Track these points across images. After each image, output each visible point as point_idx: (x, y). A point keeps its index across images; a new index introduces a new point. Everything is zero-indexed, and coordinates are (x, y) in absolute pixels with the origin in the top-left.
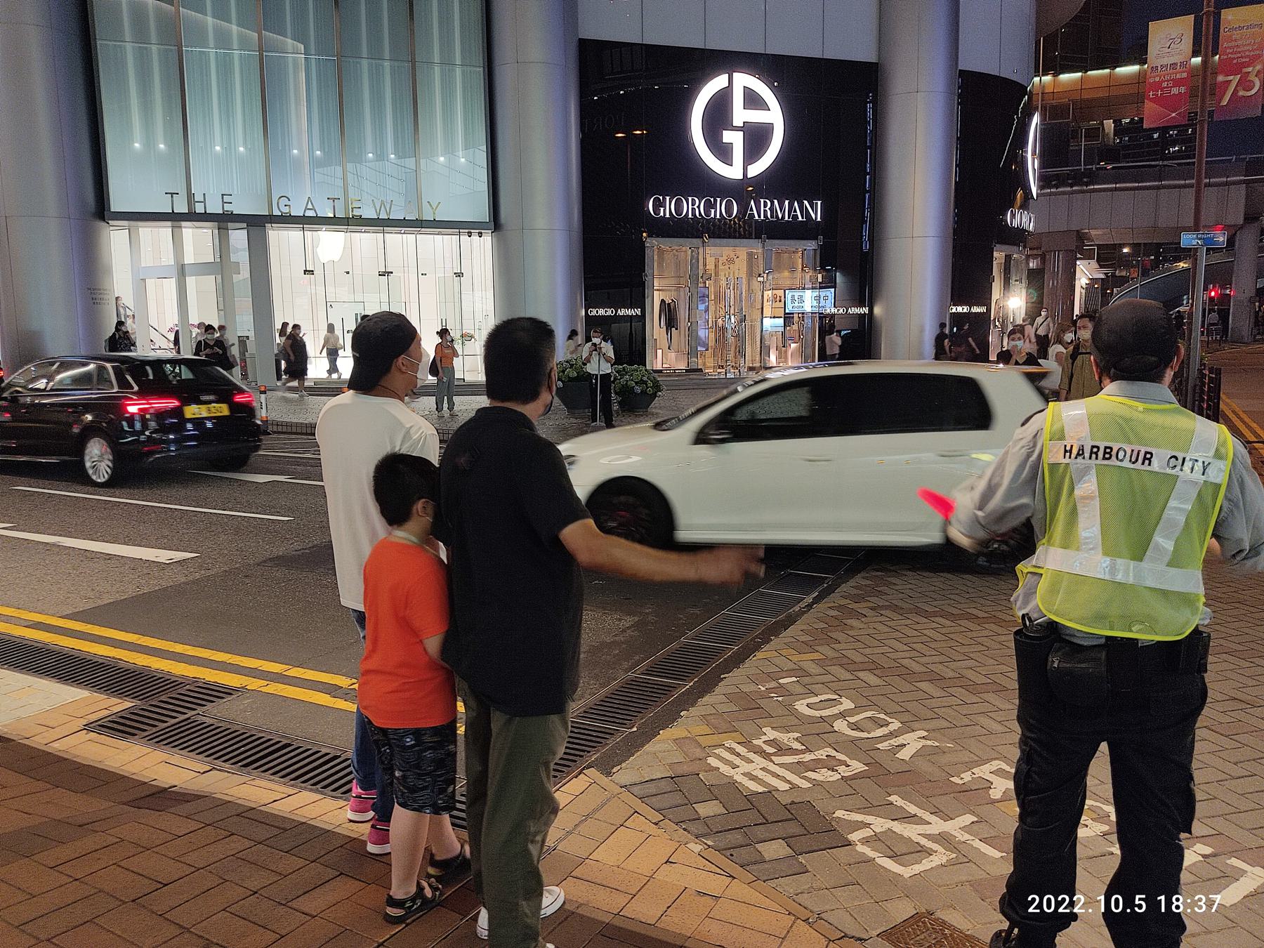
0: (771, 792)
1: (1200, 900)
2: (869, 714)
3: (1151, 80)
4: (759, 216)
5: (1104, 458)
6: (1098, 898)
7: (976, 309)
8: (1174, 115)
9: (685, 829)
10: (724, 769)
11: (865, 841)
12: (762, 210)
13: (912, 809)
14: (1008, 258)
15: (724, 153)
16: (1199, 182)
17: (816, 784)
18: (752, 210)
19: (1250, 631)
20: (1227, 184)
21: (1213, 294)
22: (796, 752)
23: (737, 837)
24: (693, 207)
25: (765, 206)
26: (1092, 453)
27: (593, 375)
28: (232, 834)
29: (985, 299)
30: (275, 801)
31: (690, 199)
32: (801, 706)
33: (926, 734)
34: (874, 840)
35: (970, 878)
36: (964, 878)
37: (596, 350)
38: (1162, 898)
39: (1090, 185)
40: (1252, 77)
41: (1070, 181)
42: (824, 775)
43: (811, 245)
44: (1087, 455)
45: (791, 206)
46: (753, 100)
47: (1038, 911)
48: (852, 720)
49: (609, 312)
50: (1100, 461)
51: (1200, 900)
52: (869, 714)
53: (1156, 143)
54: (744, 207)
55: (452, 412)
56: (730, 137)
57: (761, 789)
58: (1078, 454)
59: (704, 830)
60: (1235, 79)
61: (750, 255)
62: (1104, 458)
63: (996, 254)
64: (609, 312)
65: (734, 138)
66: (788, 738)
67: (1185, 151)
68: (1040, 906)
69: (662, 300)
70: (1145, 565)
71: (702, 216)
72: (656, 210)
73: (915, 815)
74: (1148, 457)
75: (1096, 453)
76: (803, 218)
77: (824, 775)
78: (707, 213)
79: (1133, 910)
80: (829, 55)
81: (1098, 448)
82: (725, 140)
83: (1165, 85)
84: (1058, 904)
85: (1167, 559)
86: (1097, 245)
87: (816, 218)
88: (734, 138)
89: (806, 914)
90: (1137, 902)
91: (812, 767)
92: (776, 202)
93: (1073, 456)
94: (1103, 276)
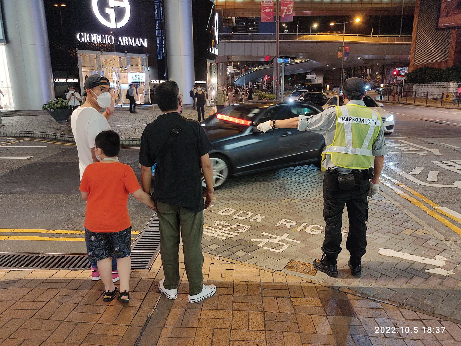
0: (229, 238)
2: (242, 212)
3: (262, 6)
5: (353, 121)
7: (203, 82)
8: (269, 18)
9: (210, 254)
10: (210, 235)
11: (264, 246)
12: (124, 41)
13: (271, 235)
14: (211, 64)
15: (107, 17)
16: (277, 40)
17: (240, 234)
18: (120, 41)
19: (299, 180)
20: (271, 42)
21: (267, 78)
22: (228, 226)
23: (228, 253)
24: (96, 38)
26: (350, 119)
27: (72, 106)
28: (48, 289)
29: (205, 80)
30: (53, 275)
32: (220, 213)
33: (260, 215)
34: (265, 245)
35: (297, 249)
36: (295, 250)
37: (73, 96)
39: (231, 40)
40: (290, 8)
41: (224, 38)
42: (240, 231)
43: (144, 56)
44: (348, 120)
47: (379, 332)
48: (238, 214)
49: (64, 80)
50: (352, 122)
51: (438, 328)
52: (242, 212)
53: (244, 27)
54: (117, 40)
55: (2, 124)
56: (108, 11)
57: (226, 238)
58: (346, 120)
59: (216, 253)
60: (286, 8)
61: (120, 58)
62: (353, 121)
63: (207, 63)
64: (64, 80)
65: (111, 12)
66: (223, 223)
67: (253, 30)
69: (86, 76)
70: (361, 149)
73: (272, 237)
74: (363, 121)
75: (351, 120)
77: (240, 231)
81: (351, 118)
83: (266, 8)
84: (386, 330)
85: (367, 147)
86: (233, 61)
88: (111, 12)
89: (261, 268)
91: (236, 229)
93: (345, 121)
94: (234, 72)
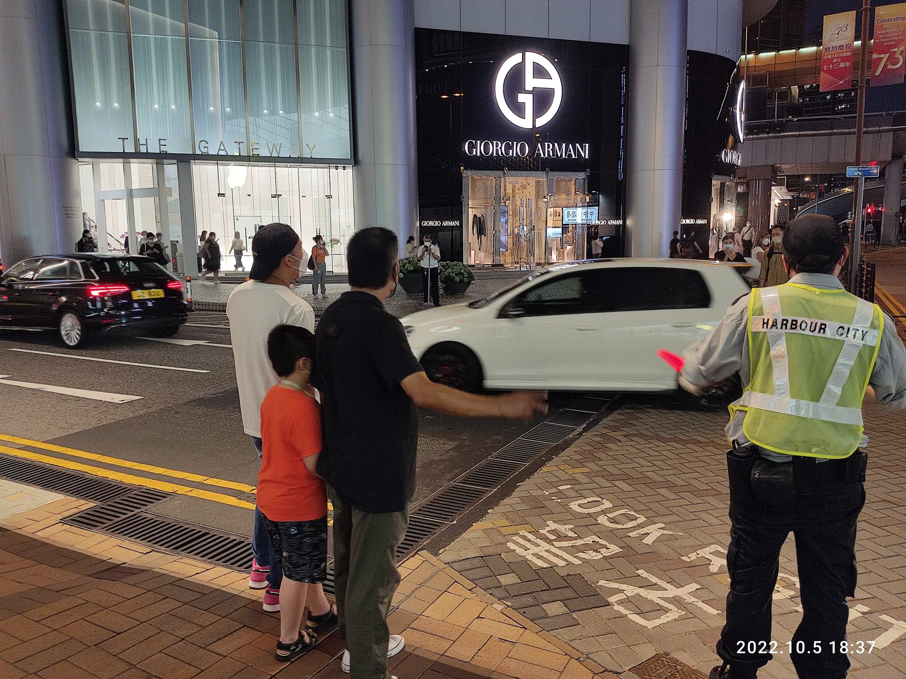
0: (552, 567)
1: (860, 644)
2: (623, 511)
3: (825, 58)
4: (544, 155)
5: (791, 328)
6: (787, 643)
7: (699, 222)
8: (841, 82)
9: (491, 594)
10: (519, 551)
11: (620, 602)
12: (546, 150)
13: (654, 579)
14: (723, 185)
15: (519, 110)
16: (859, 131)
17: (585, 561)
18: (539, 150)
19: (896, 452)
20: (879, 132)
21: (869, 210)
22: (571, 539)
23: (528, 600)
24: (497, 148)
25: (549, 147)
26: (782, 324)
27: (425, 268)
28: (166, 598)
29: (706, 214)
30: (197, 574)
31: (495, 142)
32: (574, 506)
33: (664, 525)
34: (627, 602)
35: (696, 629)
36: (691, 629)
37: (427, 251)
38: (833, 643)
39: (781, 132)
40: (897, 55)
41: (767, 130)
42: (590, 555)
43: (581, 176)
44: (779, 326)
45: (567, 147)
46: (539, 72)
47: (744, 652)
48: (611, 515)
49: (437, 224)
50: (788, 331)
51: (860, 644)
52: (623, 511)
53: (829, 103)
54: (533, 149)
55: (324, 295)
56: (523, 98)
57: (545, 565)
58: (773, 325)
59: (504, 594)
60: (885, 57)
61: (538, 183)
62: (791, 328)
63: (714, 182)
64: (437, 224)
65: (526, 99)
66: (565, 529)
67: (849, 108)
68: (745, 649)
69: (475, 215)
70: (821, 404)
71: (503, 154)
72: (470, 150)
73: (656, 584)
74: (823, 328)
75: (786, 325)
76: (575, 156)
77: (590, 555)
78: (507, 152)
79: (812, 652)
80: (594, 39)
81: (787, 321)
82: (520, 100)
83: (835, 61)
84: (759, 648)
85: (836, 400)
86: (787, 176)
87: (585, 156)
88: (526, 99)
89: (578, 655)
90: (815, 646)
91: (582, 549)
92: (556, 144)
93: (769, 326)
94: (790, 198)
